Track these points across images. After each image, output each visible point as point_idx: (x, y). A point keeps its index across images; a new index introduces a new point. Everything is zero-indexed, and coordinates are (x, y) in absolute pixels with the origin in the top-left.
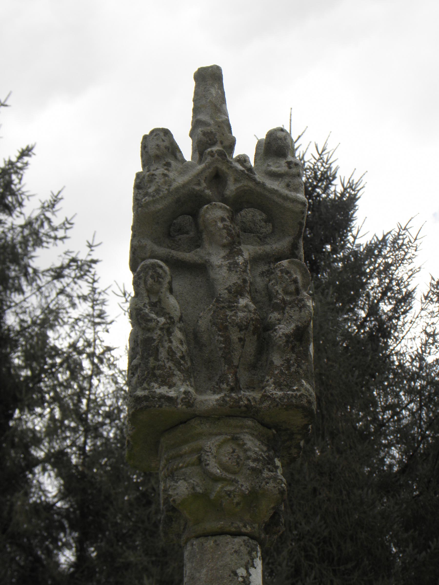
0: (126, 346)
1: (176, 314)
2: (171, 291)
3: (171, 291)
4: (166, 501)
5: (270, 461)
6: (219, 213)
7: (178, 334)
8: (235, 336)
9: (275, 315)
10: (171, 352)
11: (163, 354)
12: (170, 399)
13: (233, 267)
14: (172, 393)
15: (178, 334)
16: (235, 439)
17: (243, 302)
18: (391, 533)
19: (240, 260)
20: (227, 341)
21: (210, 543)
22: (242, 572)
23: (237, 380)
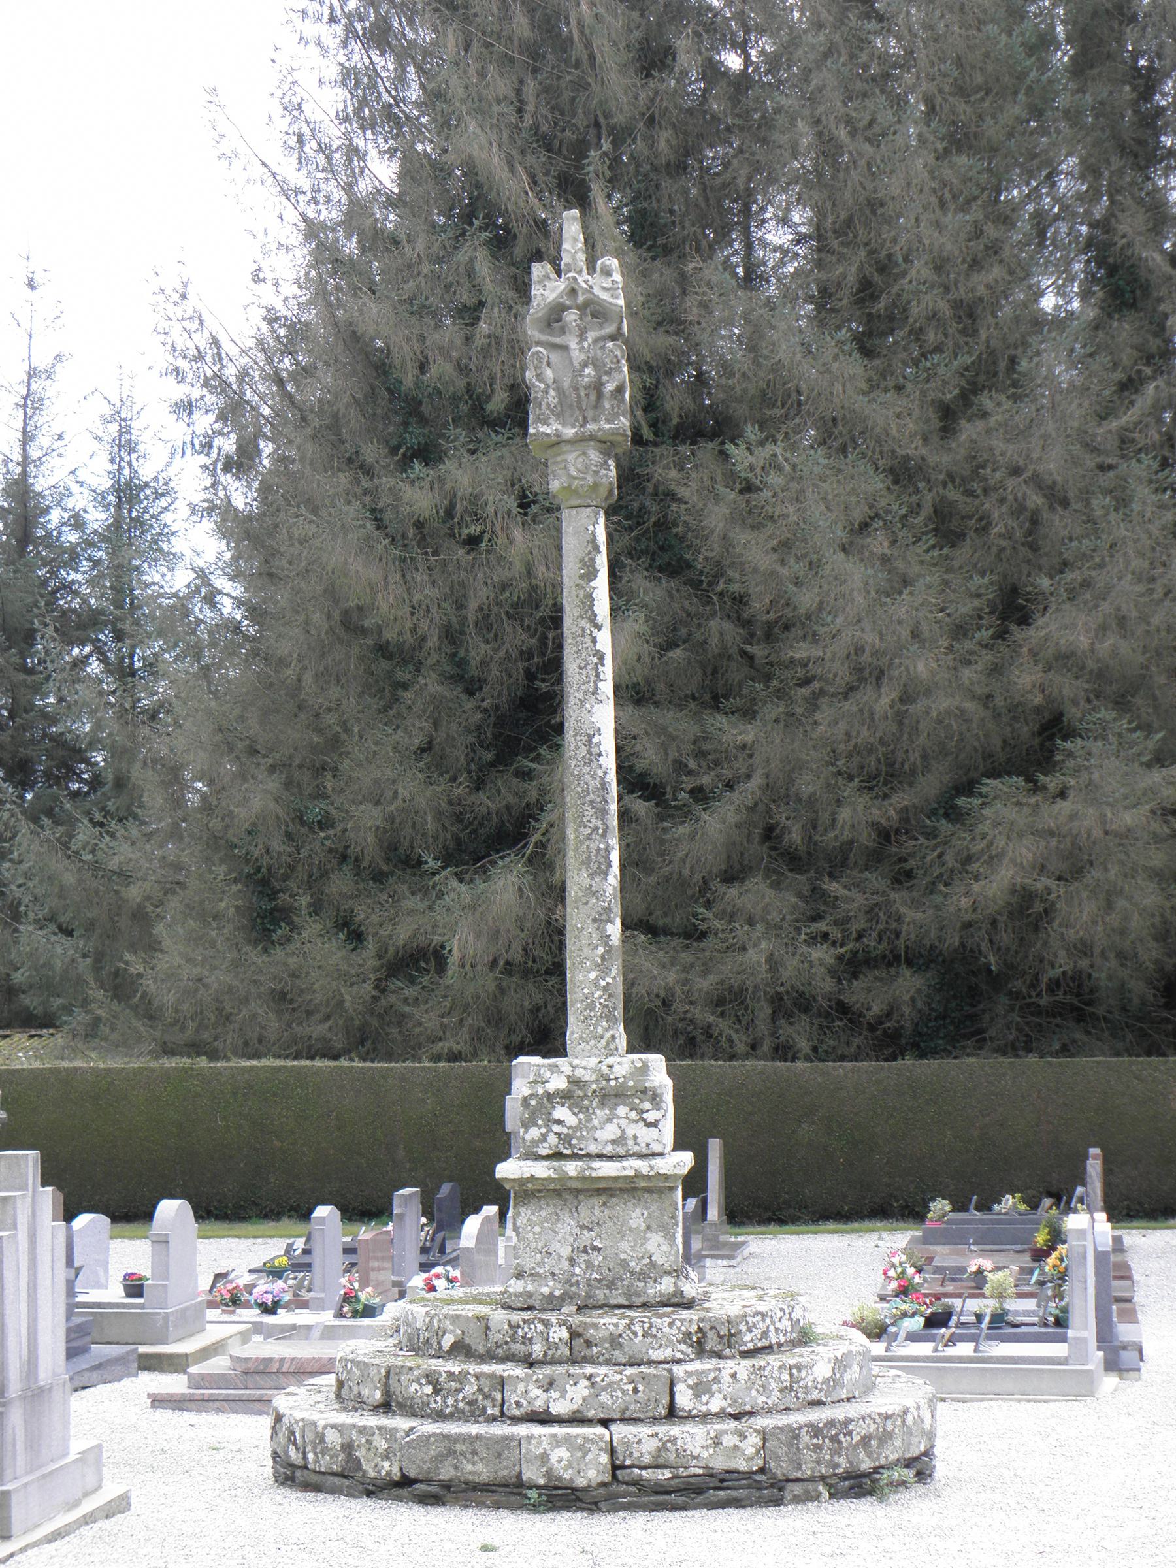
0: (158, 1401)
1: (550, 381)
2: (549, 364)
3: (549, 364)
4: (541, 845)
5: (606, 463)
6: (573, 317)
7: (552, 393)
8: (583, 393)
9: (605, 378)
10: (548, 405)
11: (544, 406)
12: (547, 435)
13: (581, 349)
14: (549, 431)
15: (552, 393)
16: (584, 453)
17: (587, 371)
18: (424, 120)
19: (586, 344)
20: (579, 396)
21: (574, 512)
22: (591, 528)
23: (585, 418)
